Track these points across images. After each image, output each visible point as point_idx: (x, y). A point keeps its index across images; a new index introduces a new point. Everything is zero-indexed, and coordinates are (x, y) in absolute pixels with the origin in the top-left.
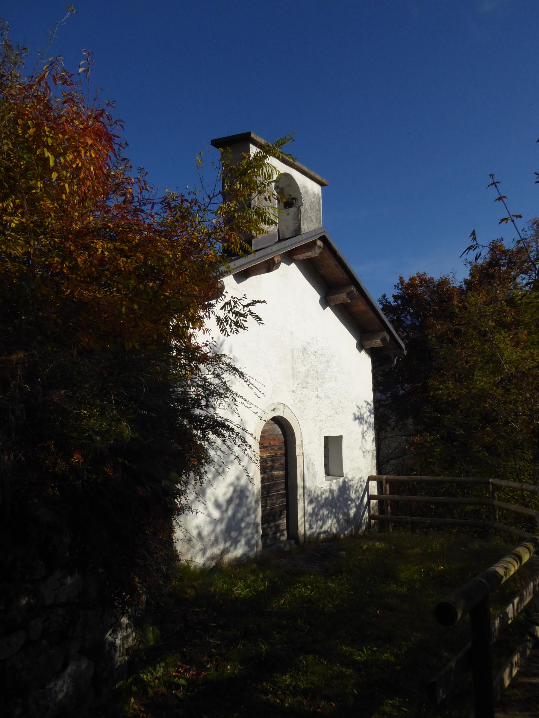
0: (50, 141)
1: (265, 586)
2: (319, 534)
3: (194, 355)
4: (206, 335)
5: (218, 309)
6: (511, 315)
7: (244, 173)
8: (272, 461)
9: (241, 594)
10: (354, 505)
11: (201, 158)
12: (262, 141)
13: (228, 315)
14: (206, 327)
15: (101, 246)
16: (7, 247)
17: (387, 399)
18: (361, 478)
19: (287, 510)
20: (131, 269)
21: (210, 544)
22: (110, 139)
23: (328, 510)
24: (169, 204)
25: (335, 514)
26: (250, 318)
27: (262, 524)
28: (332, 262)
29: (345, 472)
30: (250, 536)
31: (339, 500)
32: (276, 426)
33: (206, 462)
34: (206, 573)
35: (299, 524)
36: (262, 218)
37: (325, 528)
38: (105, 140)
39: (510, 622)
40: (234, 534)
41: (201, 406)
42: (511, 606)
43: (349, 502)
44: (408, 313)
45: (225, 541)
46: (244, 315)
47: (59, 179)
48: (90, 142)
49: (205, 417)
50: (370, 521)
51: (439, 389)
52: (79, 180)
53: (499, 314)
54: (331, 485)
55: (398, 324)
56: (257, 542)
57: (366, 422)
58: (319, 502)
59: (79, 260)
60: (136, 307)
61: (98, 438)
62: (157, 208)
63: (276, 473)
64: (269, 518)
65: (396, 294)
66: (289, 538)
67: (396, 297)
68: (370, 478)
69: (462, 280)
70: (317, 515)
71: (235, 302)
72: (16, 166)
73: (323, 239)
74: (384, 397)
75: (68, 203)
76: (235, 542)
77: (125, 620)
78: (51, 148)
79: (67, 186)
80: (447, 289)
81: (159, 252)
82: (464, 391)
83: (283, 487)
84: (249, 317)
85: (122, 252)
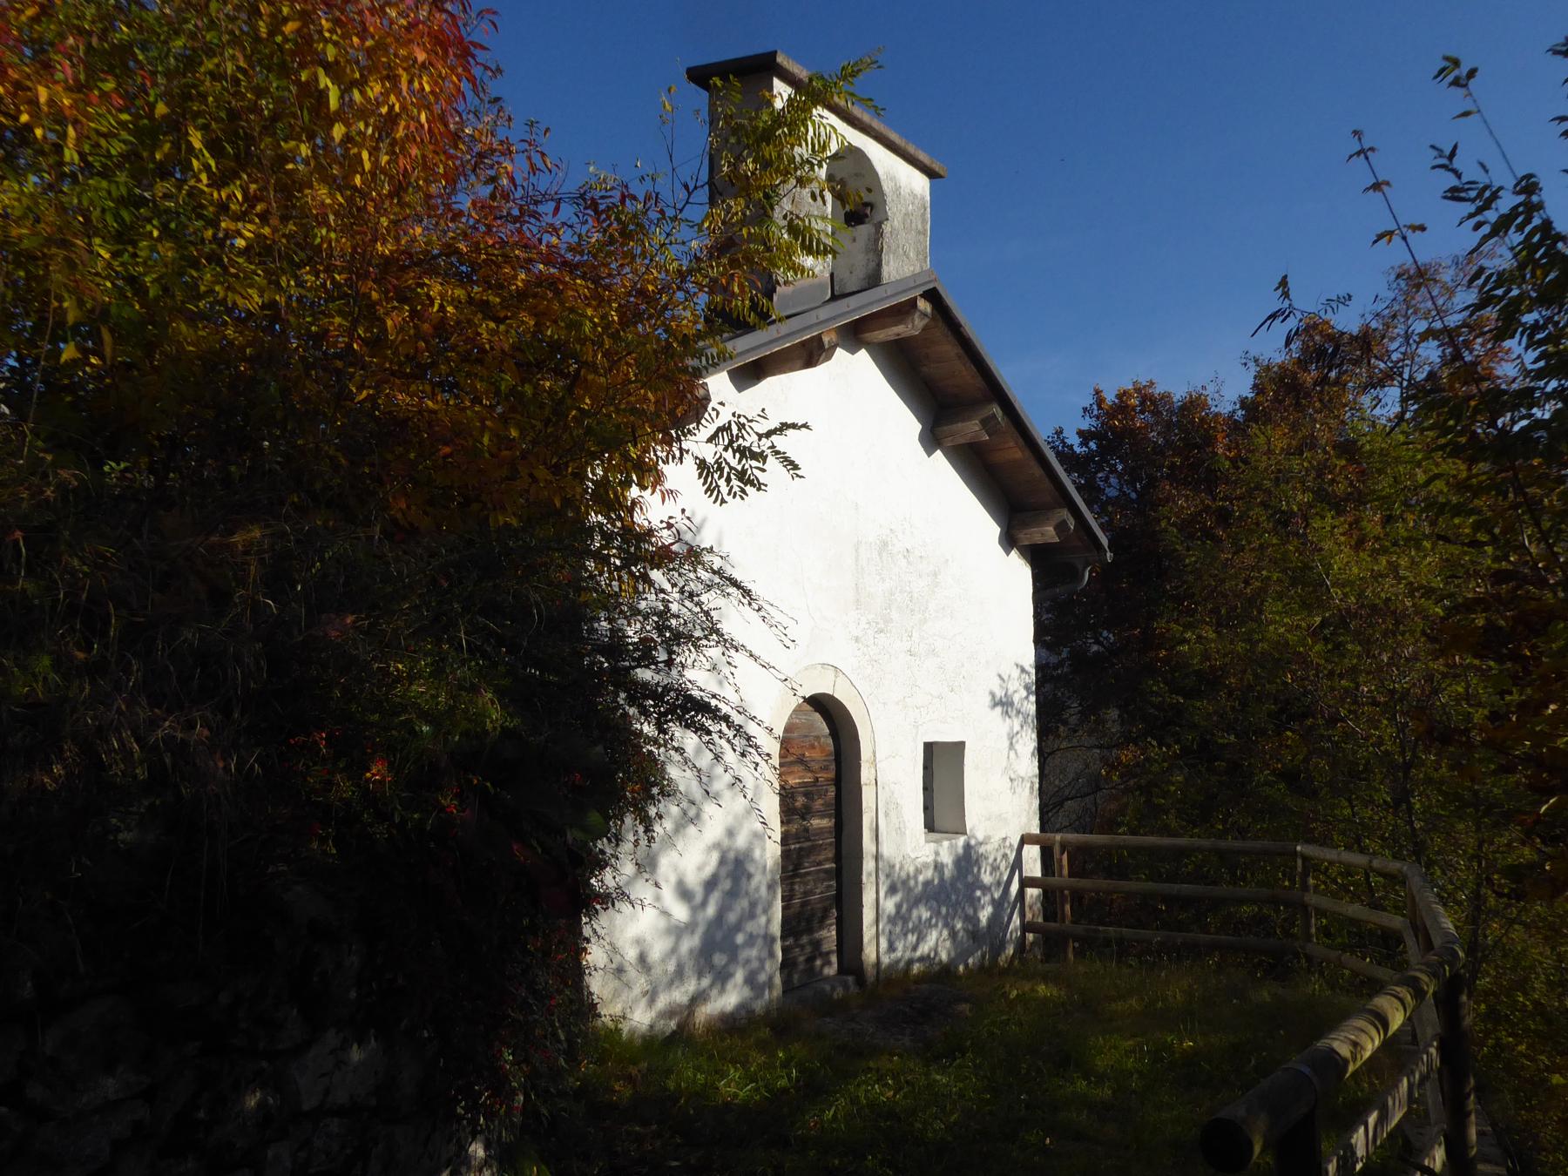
0: (331, 53)
1: (790, 1079)
2: (910, 962)
3: (642, 551)
4: (674, 499)
5: (699, 443)
6: (1346, 478)
7: (767, 136)
8: (806, 795)
9: (736, 1095)
10: (987, 898)
11: (670, 100)
12: (802, 73)
13: (725, 454)
14: (668, 485)
15: (440, 294)
16: (228, 288)
17: (1061, 664)
18: (1004, 839)
19: (839, 910)
20: (506, 347)
21: (665, 980)
22: (466, 52)
23: (930, 909)
24: (594, 205)
25: (946, 918)
26: (772, 463)
27: (783, 938)
28: (949, 349)
29: (971, 820)
30: (755, 964)
31: (953, 888)
32: (817, 716)
33: (662, 793)
34: (658, 1046)
35: (866, 940)
36: (804, 240)
37: (924, 949)
38: (455, 55)
39: (1359, 1166)
40: (719, 959)
41: (656, 664)
42: (1362, 1130)
43: (978, 893)
44: (1111, 472)
45: (700, 975)
46: (761, 457)
47: (348, 138)
48: (421, 57)
49: (665, 687)
50: (1023, 935)
51: (1184, 641)
52: (394, 143)
53: (1319, 476)
54: (937, 854)
55: (1091, 491)
56: (771, 978)
57: (1019, 712)
58: (910, 890)
59: (389, 323)
60: (514, 433)
61: (425, 728)
62: (567, 212)
63: (816, 823)
64: (797, 924)
65: (1085, 427)
66: (842, 970)
67: (1085, 436)
68: (1025, 840)
69: (1235, 398)
70: (905, 920)
71: (741, 427)
72: (255, 109)
73: (932, 296)
74: (1054, 659)
75: (364, 195)
76: (722, 978)
77: (478, 1150)
78: (332, 69)
79: (365, 155)
80: (1202, 420)
81: (572, 310)
82: (1241, 647)
83: (831, 855)
84: (771, 459)
85: (485, 308)
